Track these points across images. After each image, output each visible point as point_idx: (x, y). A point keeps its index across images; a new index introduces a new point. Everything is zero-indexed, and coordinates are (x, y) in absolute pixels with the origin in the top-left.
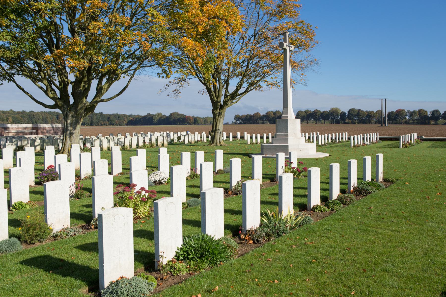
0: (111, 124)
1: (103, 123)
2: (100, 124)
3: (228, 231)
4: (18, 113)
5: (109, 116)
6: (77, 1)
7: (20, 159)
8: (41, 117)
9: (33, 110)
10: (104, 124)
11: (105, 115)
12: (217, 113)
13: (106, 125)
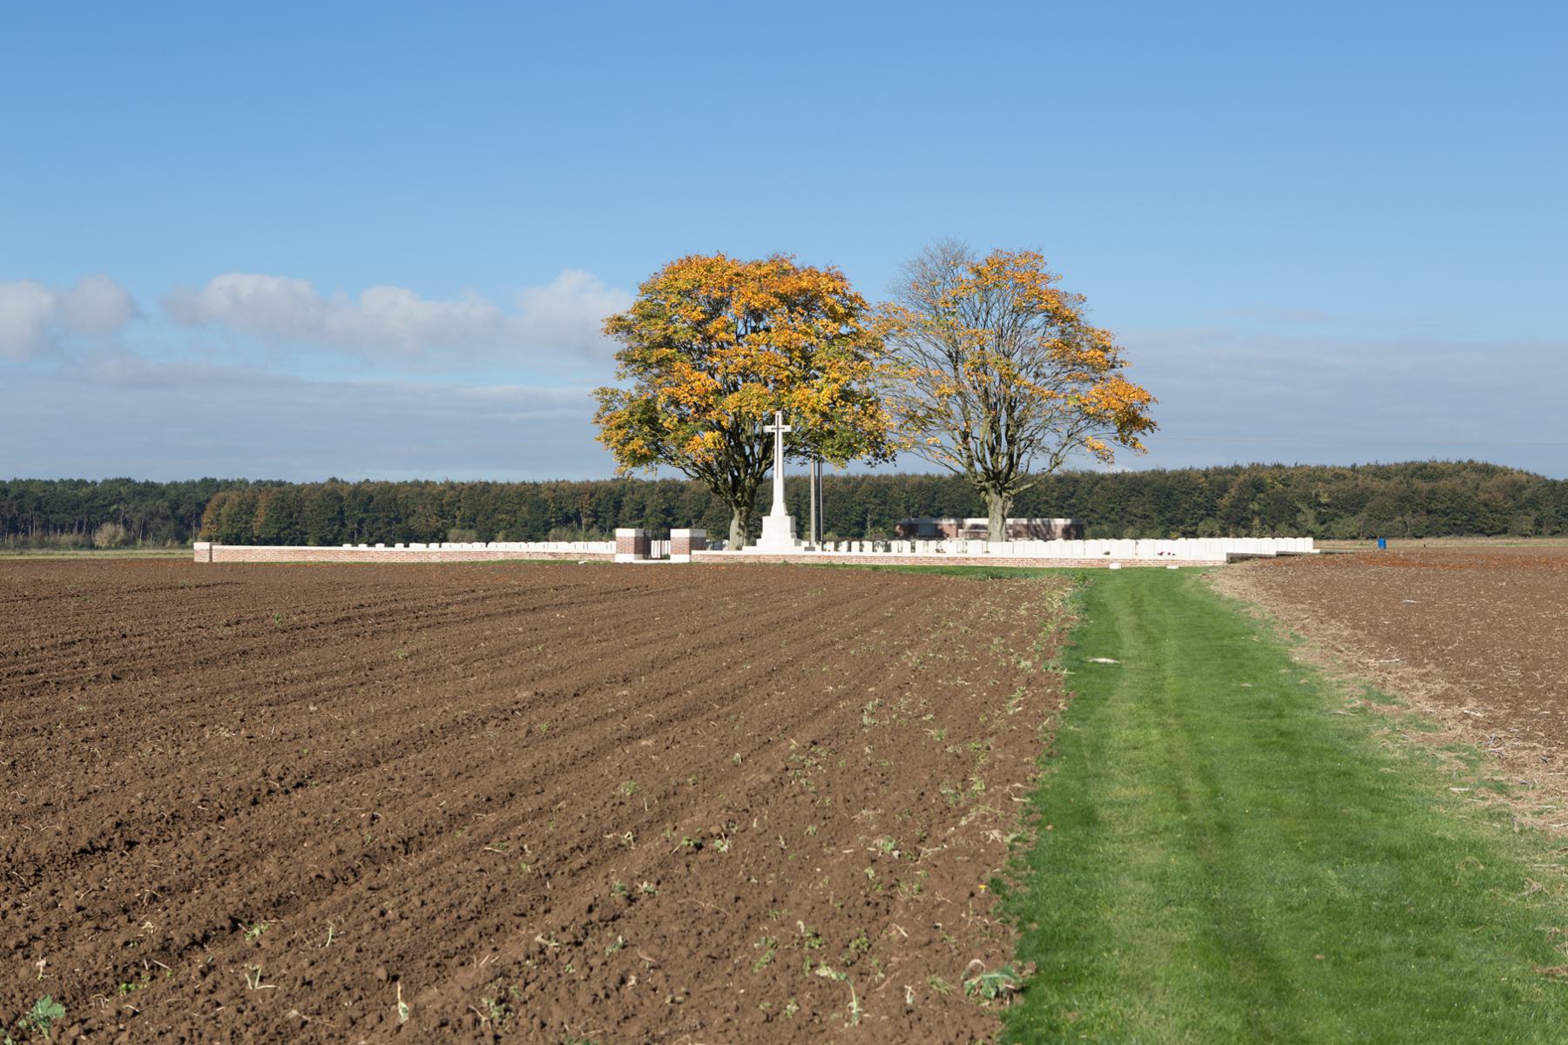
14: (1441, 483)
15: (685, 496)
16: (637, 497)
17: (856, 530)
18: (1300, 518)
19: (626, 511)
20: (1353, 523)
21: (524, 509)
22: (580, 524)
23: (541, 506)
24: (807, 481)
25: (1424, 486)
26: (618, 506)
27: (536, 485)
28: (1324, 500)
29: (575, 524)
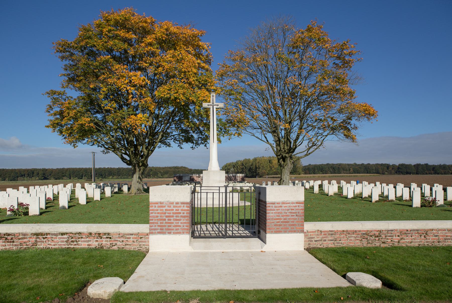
0: (436, 173)
1: (428, 173)
2: (425, 173)
3: (264, 200)
4: (359, 165)
5: (434, 166)
6: (248, 301)
7: (436, 191)
8: (374, 168)
9: (370, 163)
10: (429, 174)
11: (430, 166)
12: (99, 29)
13: (431, 174)
14: (179, 170)
15: (47, 171)
16: (37, 171)
17: (81, 177)
18: (158, 175)
19: (35, 174)
20: (166, 176)
21: (13, 174)
22: (25, 176)
23: (17, 173)
24: (92, 168)
25: (177, 170)
26: (33, 173)
27: (15, 169)
28: (162, 172)
29: (24, 176)
